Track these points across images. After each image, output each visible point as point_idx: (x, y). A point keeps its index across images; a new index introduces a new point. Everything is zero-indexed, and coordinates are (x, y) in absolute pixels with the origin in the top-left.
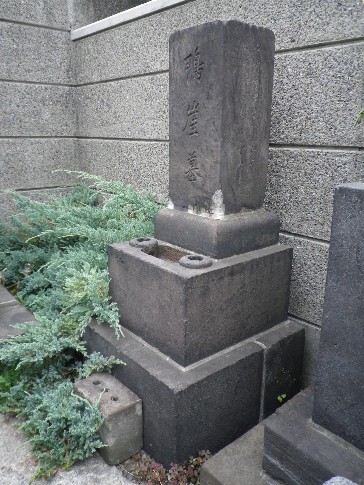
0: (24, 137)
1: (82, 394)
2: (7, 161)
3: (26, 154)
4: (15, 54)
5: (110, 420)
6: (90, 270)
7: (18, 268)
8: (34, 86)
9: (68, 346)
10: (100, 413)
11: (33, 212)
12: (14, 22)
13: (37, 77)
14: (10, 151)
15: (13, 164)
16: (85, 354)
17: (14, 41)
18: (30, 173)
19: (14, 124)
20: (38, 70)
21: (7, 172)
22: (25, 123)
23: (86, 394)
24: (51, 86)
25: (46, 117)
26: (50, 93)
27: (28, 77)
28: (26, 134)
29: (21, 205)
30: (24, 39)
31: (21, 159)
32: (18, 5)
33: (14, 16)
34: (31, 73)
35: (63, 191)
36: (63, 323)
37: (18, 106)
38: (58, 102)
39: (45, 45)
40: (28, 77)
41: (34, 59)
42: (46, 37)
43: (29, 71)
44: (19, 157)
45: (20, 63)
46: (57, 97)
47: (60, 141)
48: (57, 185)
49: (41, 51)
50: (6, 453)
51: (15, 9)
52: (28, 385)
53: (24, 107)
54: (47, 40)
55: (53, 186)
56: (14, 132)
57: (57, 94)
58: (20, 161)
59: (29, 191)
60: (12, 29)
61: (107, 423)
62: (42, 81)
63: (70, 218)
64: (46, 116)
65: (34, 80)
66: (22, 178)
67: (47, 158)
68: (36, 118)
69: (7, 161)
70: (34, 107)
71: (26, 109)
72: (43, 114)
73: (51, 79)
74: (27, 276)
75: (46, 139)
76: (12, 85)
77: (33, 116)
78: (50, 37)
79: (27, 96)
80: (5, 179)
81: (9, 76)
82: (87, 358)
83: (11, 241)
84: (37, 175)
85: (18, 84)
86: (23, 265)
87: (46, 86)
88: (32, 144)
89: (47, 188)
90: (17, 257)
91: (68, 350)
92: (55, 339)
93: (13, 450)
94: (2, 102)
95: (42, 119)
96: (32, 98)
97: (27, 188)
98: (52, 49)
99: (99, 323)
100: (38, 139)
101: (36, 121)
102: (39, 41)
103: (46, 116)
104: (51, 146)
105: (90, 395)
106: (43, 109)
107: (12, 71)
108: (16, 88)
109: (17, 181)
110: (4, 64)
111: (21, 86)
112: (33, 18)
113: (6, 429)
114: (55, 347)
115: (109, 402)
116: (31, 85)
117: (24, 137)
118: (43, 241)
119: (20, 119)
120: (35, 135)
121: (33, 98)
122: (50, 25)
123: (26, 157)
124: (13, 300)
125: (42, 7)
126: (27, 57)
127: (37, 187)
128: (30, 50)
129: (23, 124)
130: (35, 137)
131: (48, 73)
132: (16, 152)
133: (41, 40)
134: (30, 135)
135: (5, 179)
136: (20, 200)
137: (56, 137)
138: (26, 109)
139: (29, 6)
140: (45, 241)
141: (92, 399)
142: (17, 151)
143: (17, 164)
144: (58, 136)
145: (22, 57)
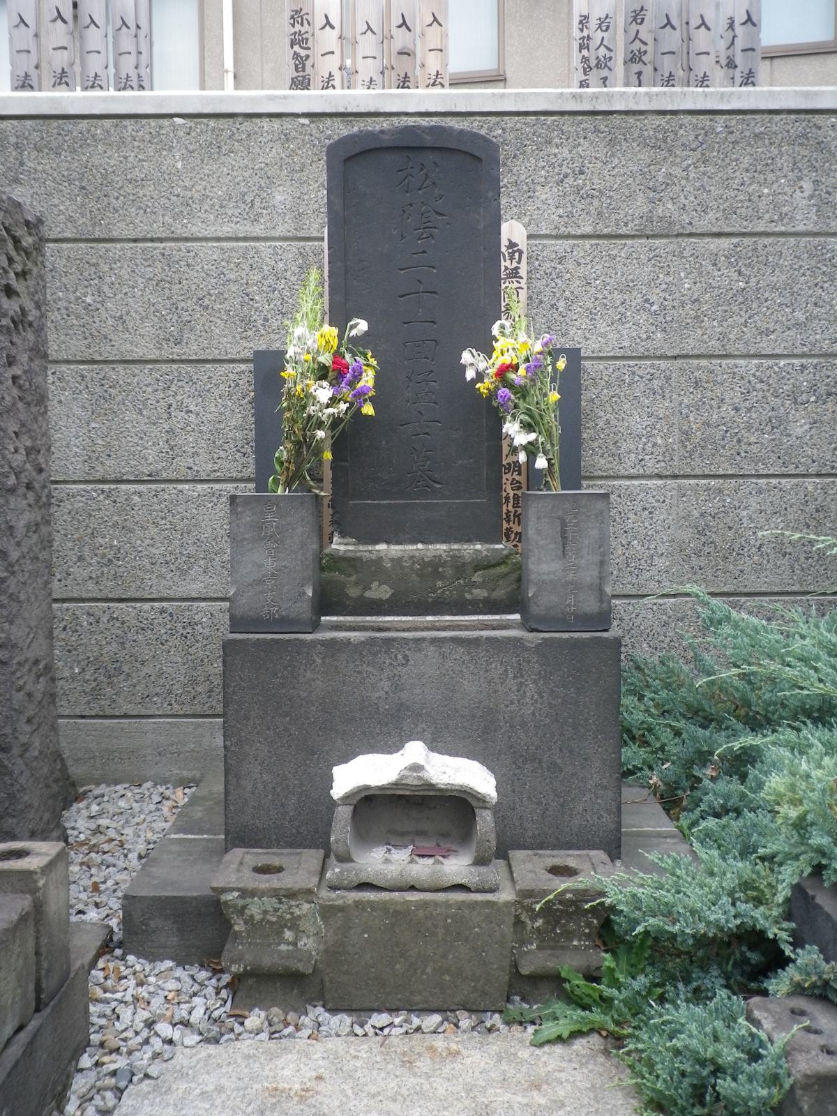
0: (743, 476)
1: (759, 1022)
2: (700, 528)
3: (745, 513)
4: (741, 300)
5: (806, 1087)
6: (821, 759)
7: (692, 762)
8: (776, 364)
9: (754, 925)
10: (786, 1065)
11: (735, 637)
12: (744, 235)
13: (786, 344)
14: (709, 507)
15: (714, 536)
16: (788, 951)
17: (740, 273)
18: (749, 556)
19: (724, 447)
20: (789, 329)
21: (698, 554)
22: (750, 444)
23: (767, 1025)
24: (815, 361)
25: (799, 431)
26: (812, 375)
27: (765, 345)
28: (749, 469)
29: (711, 620)
30: (763, 267)
31: (731, 525)
32: (756, 199)
33: (745, 223)
34: (772, 337)
35: (825, 603)
36: (754, 876)
37: (737, 409)
38: (829, 394)
39: (808, 273)
40: (765, 346)
41: (780, 305)
42: (811, 256)
43: (768, 332)
44: (728, 520)
45: (749, 318)
46: (827, 385)
47: (828, 485)
48: (812, 588)
49: (799, 286)
50: (592, 1103)
51: (747, 207)
52: (659, 990)
53: (749, 410)
54: (813, 263)
55: (802, 590)
56: (722, 465)
57: (828, 377)
58: (730, 528)
59: (743, 599)
60: (739, 249)
61: (799, 1092)
62: (795, 351)
63: (817, 659)
64: (800, 427)
65: (778, 351)
66: (731, 567)
67: (791, 525)
68: (774, 434)
69: (700, 528)
70: (773, 409)
71: (754, 415)
72: (792, 424)
73: (818, 345)
74: (706, 782)
75: (795, 481)
76: (727, 364)
77: (768, 428)
78: (822, 254)
79: (758, 386)
80: (692, 568)
81: (723, 346)
82: (789, 961)
83: (689, 706)
84: (765, 562)
85: (742, 362)
86: (703, 757)
87: (804, 361)
88: (760, 492)
89: (788, 594)
90: (694, 739)
91: (753, 937)
92: (725, 900)
93: (607, 1103)
94: (704, 403)
95: (789, 435)
96: (769, 390)
97: (738, 590)
98: (825, 279)
99: (826, 884)
100: (774, 481)
101: (773, 440)
102: (795, 267)
103: (800, 427)
104: (806, 496)
105: (776, 1027)
106: (793, 412)
107: (731, 336)
108: (736, 370)
109: (719, 573)
110: (715, 323)
111: (747, 366)
112: (786, 221)
113: (602, 1065)
114: (723, 916)
115: (814, 1053)
116: (770, 362)
117: (743, 476)
118: (758, 713)
119: (739, 435)
120: (770, 472)
121: (772, 390)
122: (825, 229)
123: (744, 520)
124: (669, 827)
125: (807, 194)
126: (766, 304)
127: (763, 589)
128: (774, 288)
129: (745, 447)
130: (767, 476)
131: (810, 332)
132: (723, 509)
133: (801, 263)
134: (757, 470)
135: (692, 568)
136: (712, 610)
137: (818, 475)
138: (754, 415)
139: (780, 196)
140: (763, 713)
141: (775, 1036)
142: (724, 506)
143: (723, 535)
144: (823, 472)
145: (754, 305)
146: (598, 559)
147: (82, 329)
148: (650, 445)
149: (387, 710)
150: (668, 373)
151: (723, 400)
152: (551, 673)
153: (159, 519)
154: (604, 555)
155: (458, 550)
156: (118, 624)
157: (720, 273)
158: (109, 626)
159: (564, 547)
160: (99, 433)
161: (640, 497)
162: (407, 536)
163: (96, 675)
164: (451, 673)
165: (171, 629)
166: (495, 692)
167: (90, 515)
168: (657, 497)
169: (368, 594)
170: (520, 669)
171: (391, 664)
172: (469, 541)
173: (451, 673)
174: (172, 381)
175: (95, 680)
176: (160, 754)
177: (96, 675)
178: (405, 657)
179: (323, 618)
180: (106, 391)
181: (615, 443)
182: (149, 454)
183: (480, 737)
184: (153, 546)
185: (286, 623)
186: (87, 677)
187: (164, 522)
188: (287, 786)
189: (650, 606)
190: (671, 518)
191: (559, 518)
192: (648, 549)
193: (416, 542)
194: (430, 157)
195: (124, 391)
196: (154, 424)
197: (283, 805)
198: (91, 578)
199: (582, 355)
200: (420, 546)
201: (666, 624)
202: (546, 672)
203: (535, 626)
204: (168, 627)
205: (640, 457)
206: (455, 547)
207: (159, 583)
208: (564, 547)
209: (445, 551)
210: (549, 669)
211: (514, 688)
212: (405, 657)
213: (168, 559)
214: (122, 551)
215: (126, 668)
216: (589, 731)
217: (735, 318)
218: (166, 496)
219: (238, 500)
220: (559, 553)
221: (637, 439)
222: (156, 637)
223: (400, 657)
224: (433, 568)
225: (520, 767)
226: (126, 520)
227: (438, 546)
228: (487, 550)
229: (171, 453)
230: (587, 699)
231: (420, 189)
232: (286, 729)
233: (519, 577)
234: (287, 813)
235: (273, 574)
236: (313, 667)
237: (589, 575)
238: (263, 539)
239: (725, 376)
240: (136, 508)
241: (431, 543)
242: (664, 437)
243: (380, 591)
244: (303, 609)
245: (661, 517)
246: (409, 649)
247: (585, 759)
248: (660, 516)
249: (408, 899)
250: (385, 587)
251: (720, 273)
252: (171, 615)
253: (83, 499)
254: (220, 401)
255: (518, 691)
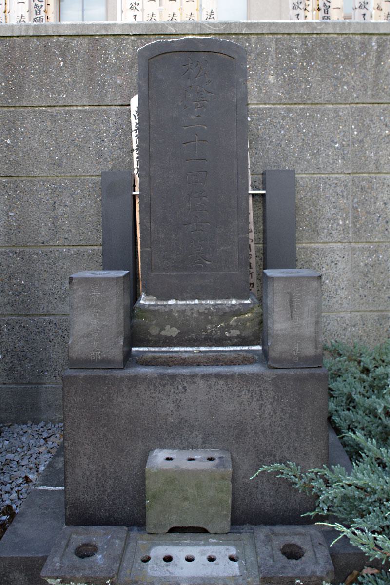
2: (365, 273)
19: (378, 225)
31: (382, 271)
66: (383, 295)
94: (366, 200)
146: (314, 320)
147: (4, 158)
148: (335, 225)
149: (172, 422)
150: (345, 183)
151: (377, 198)
152: (282, 397)
153: (48, 269)
154: (318, 318)
155: (221, 304)
156: (24, 330)
157: (375, 125)
158: (19, 331)
159: (292, 313)
160: (14, 219)
161: (329, 255)
162: (188, 295)
163: (12, 360)
164: (215, 398)
165: (55, 333)
166: (244, 410)
167: (9, 266)
168: (340, 255)
169: (163, 333)
170: (261, 395)
171: (174, 392)
172: (228, 298)
173: (215, 398)
174: (56, 188)
175: (11, 362)
176: (49, 405)
177: (12, 360)
178: (184, 387)
179: (133, 349)
180: (18, 194)
181: (315, 224)
182: (43, 231)
183: (234, 440)
184: (45, 284)
185: (106, 364)
186: (7, 361)
187: (51, 270)
188: (106, 473)
189: (336, 318)
190: (348, 267)
191: (288, 293)
192: (335, 285)
193: (194, 299)
194: (204, 56)
195: (28, 194)
196: (45, 213)
197: (103, 486)
198: (9, 303)
199: (296, 172)
200: (197, 302)
201: (345, 329)
202: (278, 397)
203: (273, 365)
204: (54, 331)
205: (330, 232)
206: (219, 302)
207: (48, 306)
208: (292, 313)
209: (213, 305)
210: (280, 394)
211: (257, 408)
212: (184, 387)
213: (53, 291)
214: (27, 287)
215: (29, 355)
216: (307, 436)
217: (384, 151)
218: (52, 255)
219: (73, 281)
220: (289, 316)
221: (328, 221)
222: (46, 337)
223: (180, 387)
224: (207, 315)
225: (261, 460)
226: (29, 269)
227: (208, 302)
228: (240, 304)
229: (55, 230)
230: (306, 414)
231: (196, 77)
232: (105, 436)
233: (261, 323)
234: (106, 491)
235: (97, 330)
236: (123, 393)
237: (308, 330)
238: (90, 307)
239: (378, 185)
240: (35, 262)
241: (204, 299)
242: (344, 220)
243: (172, 331)
244: (117, 353)
245: (342, 267)
246: (187, 382)
247: (305, 454)
248: (341, 266)
249: (217, 303)
250: (174, 329)
251: (375, 125)
252: (55, 324)
253: (4, 257)
254: (84, 200)
255: (260, 410)
